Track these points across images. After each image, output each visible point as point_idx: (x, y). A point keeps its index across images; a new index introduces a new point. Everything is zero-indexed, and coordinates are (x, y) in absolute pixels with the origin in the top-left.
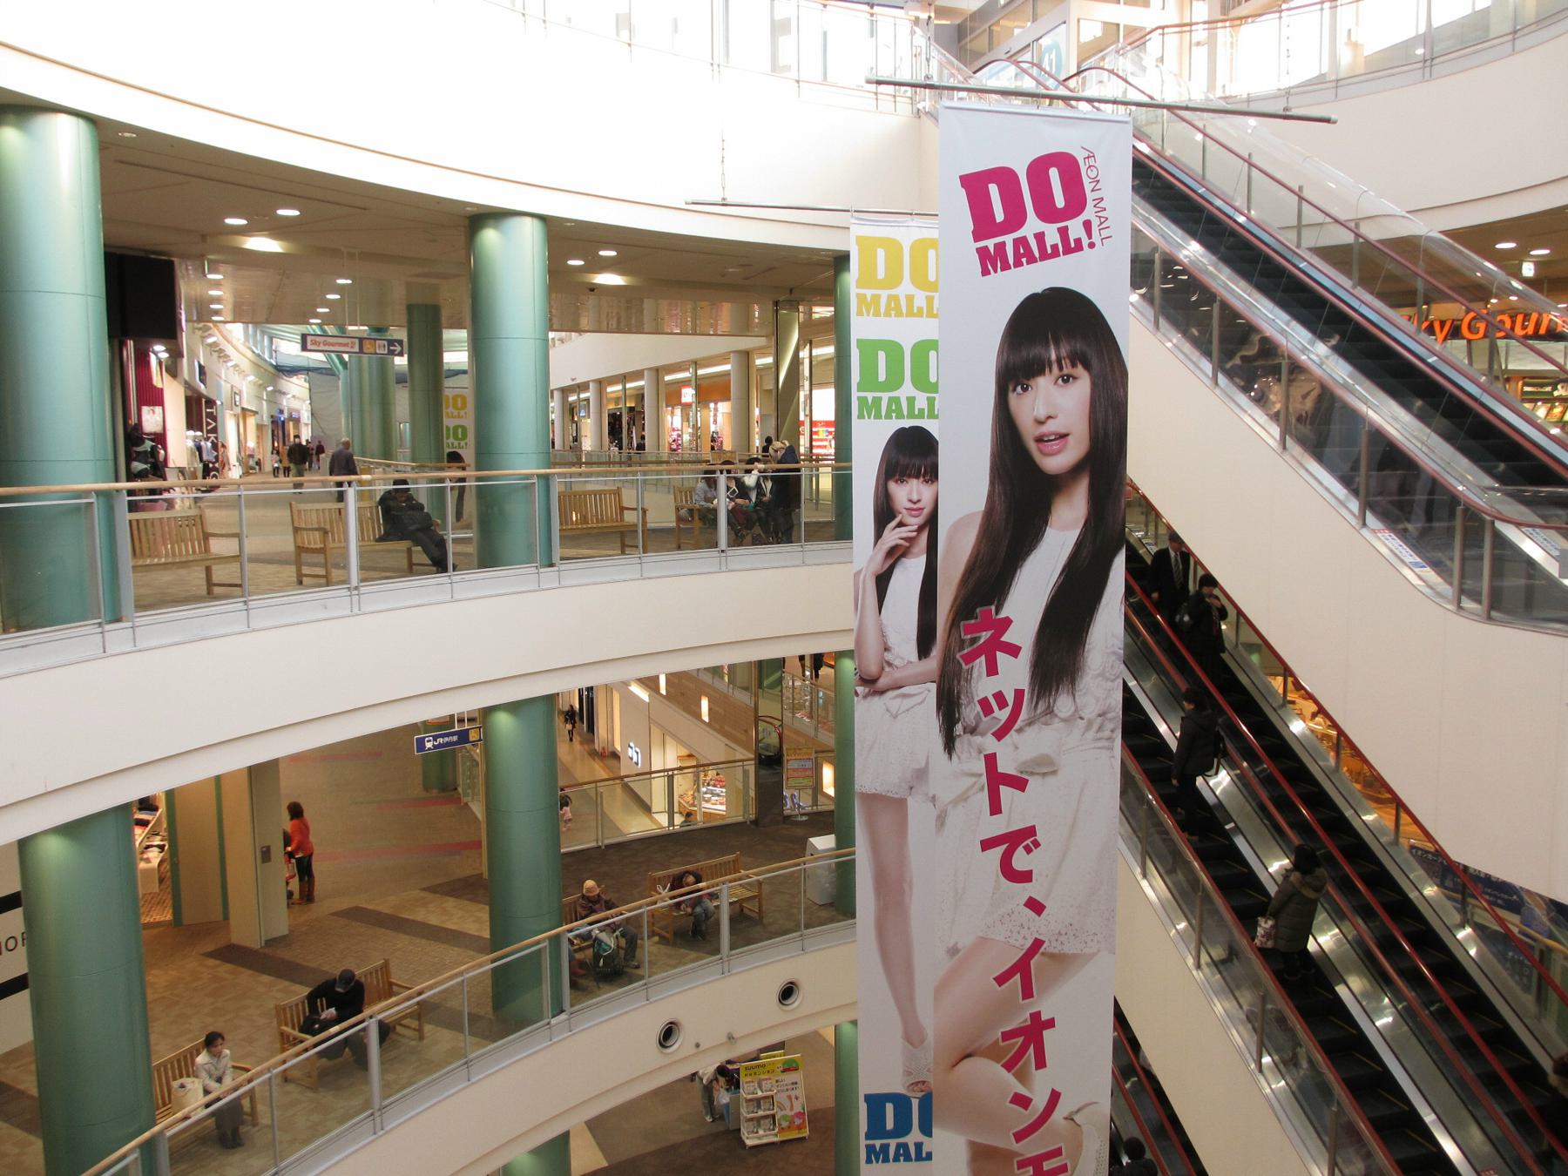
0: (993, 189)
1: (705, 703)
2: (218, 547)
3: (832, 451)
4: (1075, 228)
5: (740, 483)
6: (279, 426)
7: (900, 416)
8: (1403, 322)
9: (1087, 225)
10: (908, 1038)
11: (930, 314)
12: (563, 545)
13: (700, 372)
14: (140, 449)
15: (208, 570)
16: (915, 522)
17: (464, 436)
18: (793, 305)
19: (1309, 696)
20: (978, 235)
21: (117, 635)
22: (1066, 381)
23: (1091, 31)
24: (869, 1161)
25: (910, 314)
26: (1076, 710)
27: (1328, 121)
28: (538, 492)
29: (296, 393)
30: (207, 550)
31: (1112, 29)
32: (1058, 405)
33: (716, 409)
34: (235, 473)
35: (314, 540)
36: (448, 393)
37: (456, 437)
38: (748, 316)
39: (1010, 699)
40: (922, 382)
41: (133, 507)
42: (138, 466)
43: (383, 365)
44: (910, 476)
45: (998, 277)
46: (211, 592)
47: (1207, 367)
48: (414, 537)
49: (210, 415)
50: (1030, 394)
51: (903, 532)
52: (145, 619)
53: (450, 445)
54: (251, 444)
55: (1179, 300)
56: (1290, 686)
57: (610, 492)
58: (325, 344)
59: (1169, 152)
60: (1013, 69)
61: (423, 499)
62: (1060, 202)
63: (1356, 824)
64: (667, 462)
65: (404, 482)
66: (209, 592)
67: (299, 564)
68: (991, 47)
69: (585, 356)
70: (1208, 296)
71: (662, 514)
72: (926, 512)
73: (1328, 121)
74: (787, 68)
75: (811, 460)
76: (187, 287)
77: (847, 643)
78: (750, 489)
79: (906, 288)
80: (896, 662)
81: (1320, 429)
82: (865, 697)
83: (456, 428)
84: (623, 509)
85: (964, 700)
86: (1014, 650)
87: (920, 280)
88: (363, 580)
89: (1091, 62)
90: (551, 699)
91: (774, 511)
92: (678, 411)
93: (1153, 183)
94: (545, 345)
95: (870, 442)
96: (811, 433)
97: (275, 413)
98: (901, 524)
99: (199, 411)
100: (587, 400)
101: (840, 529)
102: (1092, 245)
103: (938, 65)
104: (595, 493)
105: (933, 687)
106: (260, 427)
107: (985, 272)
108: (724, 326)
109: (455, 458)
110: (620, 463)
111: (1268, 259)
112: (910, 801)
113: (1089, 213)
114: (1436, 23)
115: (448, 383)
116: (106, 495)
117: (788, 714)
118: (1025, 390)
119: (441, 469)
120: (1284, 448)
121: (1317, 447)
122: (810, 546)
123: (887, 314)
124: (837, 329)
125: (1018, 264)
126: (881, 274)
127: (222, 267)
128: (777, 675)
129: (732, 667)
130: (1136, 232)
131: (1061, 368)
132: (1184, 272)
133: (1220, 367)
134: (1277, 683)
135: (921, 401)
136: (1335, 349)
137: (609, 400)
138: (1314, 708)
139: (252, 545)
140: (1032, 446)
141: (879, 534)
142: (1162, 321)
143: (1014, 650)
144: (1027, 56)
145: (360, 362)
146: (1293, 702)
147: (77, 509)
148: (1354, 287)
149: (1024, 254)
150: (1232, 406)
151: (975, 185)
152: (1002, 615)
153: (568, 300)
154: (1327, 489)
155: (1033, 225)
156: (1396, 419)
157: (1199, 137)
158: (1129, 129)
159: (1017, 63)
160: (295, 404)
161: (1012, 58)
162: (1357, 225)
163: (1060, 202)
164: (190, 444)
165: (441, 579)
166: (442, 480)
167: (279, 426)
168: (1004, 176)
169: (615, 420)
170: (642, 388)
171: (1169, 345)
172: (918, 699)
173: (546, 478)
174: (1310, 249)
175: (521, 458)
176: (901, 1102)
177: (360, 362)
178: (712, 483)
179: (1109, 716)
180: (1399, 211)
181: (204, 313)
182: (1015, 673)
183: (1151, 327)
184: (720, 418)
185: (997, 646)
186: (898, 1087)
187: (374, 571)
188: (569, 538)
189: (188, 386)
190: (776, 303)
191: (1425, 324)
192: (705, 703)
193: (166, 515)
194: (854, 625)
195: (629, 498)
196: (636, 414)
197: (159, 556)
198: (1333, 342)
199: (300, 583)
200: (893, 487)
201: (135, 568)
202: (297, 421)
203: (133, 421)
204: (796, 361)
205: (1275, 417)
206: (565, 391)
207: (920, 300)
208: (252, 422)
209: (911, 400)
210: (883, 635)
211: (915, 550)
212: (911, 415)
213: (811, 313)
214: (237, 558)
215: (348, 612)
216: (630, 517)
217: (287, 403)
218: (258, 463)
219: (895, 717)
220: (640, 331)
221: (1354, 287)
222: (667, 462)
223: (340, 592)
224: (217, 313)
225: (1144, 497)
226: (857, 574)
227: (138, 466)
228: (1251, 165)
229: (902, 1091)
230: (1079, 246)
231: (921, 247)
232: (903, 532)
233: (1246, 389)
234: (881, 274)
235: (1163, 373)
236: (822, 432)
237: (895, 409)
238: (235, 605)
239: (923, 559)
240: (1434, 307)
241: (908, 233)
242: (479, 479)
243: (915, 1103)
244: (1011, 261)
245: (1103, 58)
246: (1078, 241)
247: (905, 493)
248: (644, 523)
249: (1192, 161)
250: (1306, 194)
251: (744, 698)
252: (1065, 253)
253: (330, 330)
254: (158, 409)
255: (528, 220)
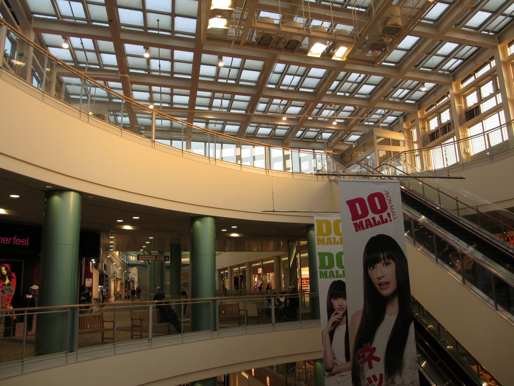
0: (357, 205)
1: (268, 379)
2: (107, 325)
3: (309, 288)
4: (385, 215)
5: (279, 301)
6: (127, 284)
7: (334, 277)
8: (497, 238)
9: (389, 214)
11: (341, 244)
12: (220, 323)
13: (264, 263)
14: (84, 292)
15: (103, 334)
16: (341, 313)
17: (187, 286)
18: (294, 241)
19: (486, 372)
20: (353, 219)
21: (72, 356)
22: (387, 265)
23: (382, 154)
26: (403, 381)
27: (462, 178)
28: (212, 305)
29: (134, 272)
30: (103, 326)
31: (389, 153)
32: (385, 272)
33: (269, 275)
34: (113, 299)
35: (138, 323)
36: (182, 272)
37: (184, 286)
38: (279, 244)
39: (378, 377)
40: (340, 265)
41: (81, 312)
42: (83, 298)
43: (162, 263)
44: (339, 297)
45: (361, 232)
46: (103, 341)
47: (434, 257)
48: (171, 322)
49: (106, 281)
50: (375, 270)
51: (337, 316)
52: (80, 351)
53: (183, 289)
54: (118, 290)
55: (421, 235)
56: (480, 369)
57: (235, 304)
58: (145, 258)
59: (411, 188)
60: (359, 166)
61: (173, 308)
62: (379, 208)
63: (446, 350)
64: (254, 294)
65: (168, 303)
66: (103, 341)
67: (132, 331)
68: (351, 160)
69: (226, 259)
70: (431, 233)
71: (253, 312)
72: (345, 309)
73: (462, 178)
74: (289, 169)
75: (302, 292)
76: (103, 241)
77: (320, 356)
78: (282, 303)
79: (333, 235)
80: (338, 363)
81: (474, 275)
82: (328, 376)
83: (184, 283)
84: (239, 310)
85: (361, 378)
86: (378, 359)
87: (337, 233)
88: (153, 336)
89: (384, 162)
90: (215, 378)
91: (291, 309)
92: (257, 276)
93: (409, 199)
94: (215, 255)
95: (324, 286)
96: (301, 282)
97: (127, 279)
98: (336, 314)
99: (103, 279)
100: (227, 273)
101: (313, 314)
102: (391, 220)
103: (335, 167)
104: (229, 305)
105: (350, 372)
106: (121, 284)
107: (357, 231)
108: (271, 248)
109: (184, 294)
110: (238, 295)
111: (449, 221)
113: (389, 210)
114: (492, 145)
115: (183, 268)
116: (73, 309)
117: (298, 383)
118: (373, 268)
119: (180, 298)
120: (464, 283)
121: (475, 283)
122: (303, 322)
123: (327, 244)
124: (310, 248)
125: (367, 227)
126: (325, 231)
127: (114, 235)
128: (292, 368)
129: (277, 366)
130: (404, 214)
131: (385, 261)
132: (421, 225)
133: (438, 257)
134: (475, 368)
135: (340, 272)
136: (476, 248)
137: (234, 273)
138: (490, 377)
139: (118, 324)
140: (378, 287)
141: (329, 317)
142: (416, 242)
143: (378, 359)
144: (363, 162)
145: (155, 263)
146: (482, 375)
147: (63, 314)
148: (480, 228)
149: (369, 224)
150: (443, 268)
151: (351, 204)
152: (373, 346)
153: (222, 242)
154: (481, 296)
155: (371, 215)
156: (501, 271)
157: (421, 183)
158: (399, 184)
159: (360, 164)
160: (133, 276)
161: (358, 163)
162: (477, 208)
163: (379, 208)
164: (99, 290)
165: (179, 335)
166: (180, 302)
167: (127, 284)
168: (360, 201)
169: (236, 279)
170: (245, 269)
171: (419, 249)
173: (214, 301)
174: (462, 216)
175: (206, 295)
177: (155, 263)
178: (269, 301)
179: (415, 383)
180: (490, 203)
181: (107, 248)
182: (379, 368)
183: (413, 244)
184: (270, 278)
185: (372, 358)
187: (157, 333)
188: (222, 321)
189: (101, 271)
190: (288, 241)
191: (506, 239)
192: (268, 379)
193: (91, 315)
194: (323, 349)
195: (241, 307)
196: (243, 278)
197: (87, 328)
198: (475, 246)
199: (132, 337)
200: (333, 301)
201: (79, 333)
202: (133, 282)
203: (83, 283)
204: (295, 259)
205: (459, 272)
206: (220, 270)
207: (338, 239)
208: (119, 282)
209: (337, 272)
210: (333, 353)
211: (342, 322)
212: (337, 277)
213: (299, 243)
214: (113, 329)
215: (147, 348)
216: (242, 313)
217: (131, 275)
218: (120, 296)
219: (339, 384)
220: (244, 250)
221: (480, 228)
222: (254, 294)
223: (145, 341)
224: (111, 248)
225: (417, 301)
226: (323, 332)
227: (83, 298)
228: (439, 191)
230: (386, 221)
231: (337, 222)
232: (337, 316)
233: (447, 263)
234: (325, 231)
235: (416, 256)
236: (305, 282)
237: (332, 275)
238: (110, 346)
239: (345, 325)
240: (508, 233)
241: (332, 218)
242: (192, 301)
244: (365, 226)
245: (387, 161)
246: (386, 219)
247: (336, 303)
248: (247, 315)
249: (420, 191)
250: (458, 199)
251: (281, 377)
252: (382, 223)
253: (146, 253)
254: (91, 279)
255: (210, 218)
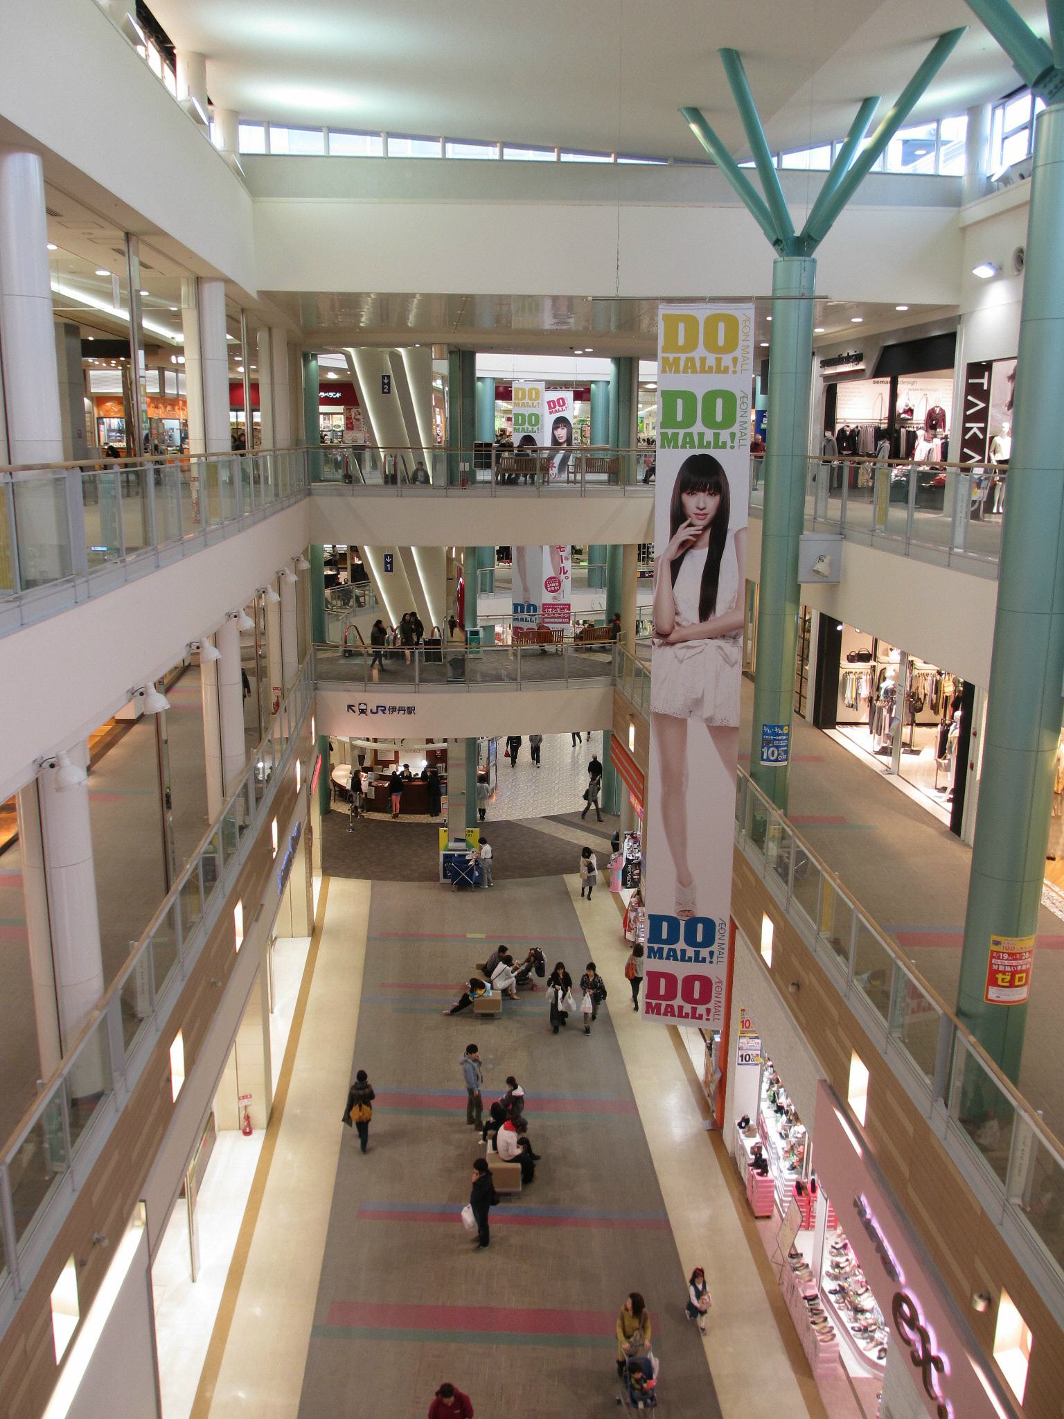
7: (693, 447)
10: (680, 881)
16: (701, 523)
24: (649, 957)
25: (703, 371)
51: (692, 530)
80: (684, 623)
82: (660, 646)
98: (691, 525)
102: (735, 372)
112: (690, 721)
141: (674, 531)
155: (700, 352)
172: (700, 649)
176: (673, 922)
186: (671, 912)
200: (685, 497)
212: (701, 446)
229: (674, 915)
230: (726, 370)
232: (692, 530)
237: (689, 441)
243: (682, 924)
